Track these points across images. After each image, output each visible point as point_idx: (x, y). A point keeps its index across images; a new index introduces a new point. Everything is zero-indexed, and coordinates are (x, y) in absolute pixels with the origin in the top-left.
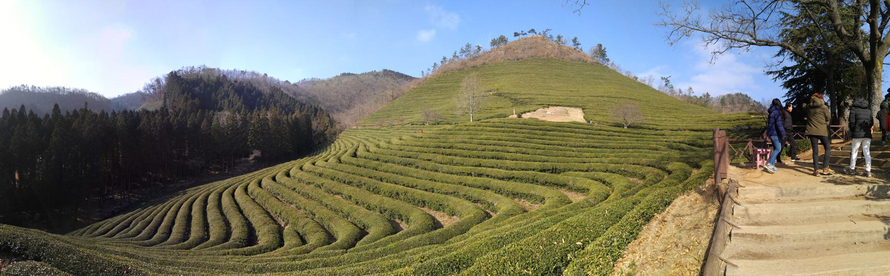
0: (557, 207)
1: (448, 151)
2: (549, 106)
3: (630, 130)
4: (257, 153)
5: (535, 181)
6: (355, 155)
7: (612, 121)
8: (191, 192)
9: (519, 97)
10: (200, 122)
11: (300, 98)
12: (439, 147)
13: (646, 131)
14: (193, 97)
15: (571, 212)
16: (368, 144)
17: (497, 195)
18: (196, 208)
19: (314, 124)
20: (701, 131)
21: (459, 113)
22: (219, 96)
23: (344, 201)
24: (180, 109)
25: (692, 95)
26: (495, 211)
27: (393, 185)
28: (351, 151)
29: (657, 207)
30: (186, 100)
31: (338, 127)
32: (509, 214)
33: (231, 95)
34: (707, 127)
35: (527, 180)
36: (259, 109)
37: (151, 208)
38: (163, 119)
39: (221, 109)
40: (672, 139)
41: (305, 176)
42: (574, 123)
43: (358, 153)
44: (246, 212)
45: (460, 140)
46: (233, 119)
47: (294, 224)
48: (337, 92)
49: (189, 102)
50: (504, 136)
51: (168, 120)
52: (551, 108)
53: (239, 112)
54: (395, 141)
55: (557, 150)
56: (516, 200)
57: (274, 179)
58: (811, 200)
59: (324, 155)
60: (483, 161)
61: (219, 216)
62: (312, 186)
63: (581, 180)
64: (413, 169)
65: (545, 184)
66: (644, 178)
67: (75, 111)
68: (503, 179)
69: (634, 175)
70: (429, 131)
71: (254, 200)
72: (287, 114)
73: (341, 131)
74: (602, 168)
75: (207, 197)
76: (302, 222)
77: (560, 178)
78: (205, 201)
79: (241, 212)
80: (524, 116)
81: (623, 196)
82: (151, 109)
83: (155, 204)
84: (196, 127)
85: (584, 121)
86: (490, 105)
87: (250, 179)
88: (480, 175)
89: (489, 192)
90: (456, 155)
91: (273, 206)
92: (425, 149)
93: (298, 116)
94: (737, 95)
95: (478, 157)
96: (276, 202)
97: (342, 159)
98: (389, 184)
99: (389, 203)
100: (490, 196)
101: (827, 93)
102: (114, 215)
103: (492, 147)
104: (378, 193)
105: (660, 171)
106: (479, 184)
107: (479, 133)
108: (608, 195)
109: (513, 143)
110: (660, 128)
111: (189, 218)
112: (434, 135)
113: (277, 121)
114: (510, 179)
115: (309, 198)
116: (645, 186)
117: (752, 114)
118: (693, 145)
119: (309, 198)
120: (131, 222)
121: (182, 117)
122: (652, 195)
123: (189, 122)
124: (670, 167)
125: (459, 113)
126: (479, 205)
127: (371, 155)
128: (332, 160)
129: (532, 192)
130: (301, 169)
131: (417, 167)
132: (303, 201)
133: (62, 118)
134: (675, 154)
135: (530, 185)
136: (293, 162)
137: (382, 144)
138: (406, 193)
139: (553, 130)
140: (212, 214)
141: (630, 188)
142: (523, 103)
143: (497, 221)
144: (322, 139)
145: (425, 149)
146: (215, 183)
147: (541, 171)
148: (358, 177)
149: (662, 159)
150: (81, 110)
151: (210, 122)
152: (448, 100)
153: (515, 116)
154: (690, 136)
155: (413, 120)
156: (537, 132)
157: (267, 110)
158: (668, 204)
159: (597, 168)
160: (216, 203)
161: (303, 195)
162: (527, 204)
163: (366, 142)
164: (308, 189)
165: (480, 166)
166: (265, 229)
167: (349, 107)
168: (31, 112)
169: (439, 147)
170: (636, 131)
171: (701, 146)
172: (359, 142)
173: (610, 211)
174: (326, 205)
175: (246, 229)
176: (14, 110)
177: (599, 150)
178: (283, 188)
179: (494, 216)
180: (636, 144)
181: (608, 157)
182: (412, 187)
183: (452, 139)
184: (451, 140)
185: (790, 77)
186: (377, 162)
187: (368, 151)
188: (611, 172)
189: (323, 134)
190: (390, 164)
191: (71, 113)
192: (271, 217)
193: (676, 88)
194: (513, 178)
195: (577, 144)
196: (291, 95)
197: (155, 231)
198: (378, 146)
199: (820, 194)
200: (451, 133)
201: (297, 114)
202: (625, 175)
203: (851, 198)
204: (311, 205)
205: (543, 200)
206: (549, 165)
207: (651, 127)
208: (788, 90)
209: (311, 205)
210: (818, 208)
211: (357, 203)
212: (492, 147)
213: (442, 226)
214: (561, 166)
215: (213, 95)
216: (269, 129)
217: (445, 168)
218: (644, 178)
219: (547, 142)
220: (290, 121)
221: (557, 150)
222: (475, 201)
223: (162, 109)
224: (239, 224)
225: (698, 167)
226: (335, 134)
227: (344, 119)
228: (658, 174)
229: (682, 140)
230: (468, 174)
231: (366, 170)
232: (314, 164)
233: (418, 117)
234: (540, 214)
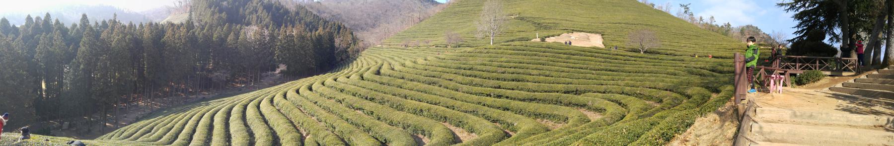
0: (577, 126)
1: (468, 72)
2: (573, 31)
3: (646, 55)
4: (283, 67)
5: (558, 102)
6: (378, 73)
7: (628, 47)
8: (214, 104)
9: (542, 21)
10: (227, 36)
11: (323, 16)
12: (460, 68)
13: (664, 57)
14: (221, 11)
15: (591, 130)
16: (393, 62)
17: (517, 116)
18: (218, 119)
19: (337, 42)
20: (721, 58)
21: (479, 36)
22: (248, 11)
23: (366, 116)
24: (206, 23)
25: (714, 24)
26: (515, 131)
27: (418, 102)
28: (374, 68)
29: (677, 128)
30: (213, 14)
31: (361, 44)
32: (529, 133)
33: (260, 12)
34: (727, 54)
35: (551, 102)
36: (286, 26)
37: (172, 116)
38: (188, 32)
39: (248, 24)
40: (693, 64)
41: (326, 91)
42: (594, 48)
43: (382, 71)
44: (271, 123)
45: (480, 62)
46: (261, 34)
47: (315, 135)
48: (362, 11)
49: (216, 16)
50: (526, 59)
51: (194, 33)
52: (575, 33)
53: (267, 28)
54: (420, 61)
55: (578, 73)
56: (539, 120)
57: (298, 92)
58: (827, 125)
59: (346, 71)
60: (502, 83)
61: (243, 127)
62: (333, 101)
63: (599, 101)
64: (436, 87)
65: (569, 104)
66: (661, 101)
67: (104, 22)
68: (524, 100)
69: (650, 98)
70: (449, 54)
71: (279, 110)
72: (311, 31)
73: (364, 49)
74: (618, 90)
75: (231, 109)
76: (322, 135)
77: (581, 98)
78: (229, 113)
79: (266, 122)
80: (547, 39)
81: (639, 117)
82: (176, 22)
83: (177, 112)
84: (223, 40)
85: (602, 46)
86: (511, 28)
87: (276, 91)
88: (499, 97)
89: (508, 113)
90: (475, 76)
91: (296, 116)
92: (448, 70)
93: (322, 33)
94: (748, 26)
95: (498, 79)
96: (299, 113)
97: (365, 76)
98: (414, 102)
99: (413, 119)
100: (509, 117)
101: (839, 26)
102: (138, 120)
103: (512, 70)
104: (402, 110)
105: (678, 96)
106: (498, 105)
107: (499, 55)
108: (624, 116)
109: (535, 66)
110: (679, 53)
111: (211, 128)
112: (455, 57)
113: (302, 38)
114: (531, 100)
115: (330, 111)
116: (663, 109)
117: (761, 45)
118: (713, 71)
119: (330, 111)
120: (152, 128)
121: (208, 30)
122: (672, 117)
123: (215, 36)
124: (689, 92)
125: (479, 36)
126: (498, 124)
127: (395, 74)
128: (354, 77)
129: (556, 113)
130: (323, 84)
131: (440, 86)
132: (324, 114)
133: (91, 28)
134: (696, 79)
135: (554, 106)
136: (315, 77)
137: (408, 63)
138: (429, 110)
139: (577, 54)
140: (235, 125)
141: (646, 110)
142: (546, 28)
143: (517, 139)
144: (344, 57)
145: (448, 70)
146: (241, 96)
147: (565, 93)
148: (380, 94)
149: (681, 83)
150: (110, 20)
151: (237, 35)
152: (469, 24)
153: (538, 40)
154: (711, 62)
155: (437, 42)
156: (562, 55)
157: (293, 27)
158: (689, 125)
159: (614, 90)
160: (240, 115)
161: (324, 109)
162: (550, 124)
163: (391, 61)
164: (329, 103)
165: (499, 87)
166: (289, 137)
167: (373, 26)
168: (57, 22)
169: (460, 68)
170: (652, 56)
171: (721, 72)
172: (383, 60)
173: (628, 130)
174: (347, 120)
175: (270, 138)
176: (38, 18)
177: (615, 73)
178: (306, 101)
179: (514, 135)
180: (652, 69)
181: (624, 80)
182: (435, 104)
183: (471, 62)
184: (472, 62)
185: (802, 9)
186: (402, 81)
187: (393, 69)
188: (627, 94)
189: (345, 51)
190: (415, 83)
191: (100, 24)
192: (295, 126)
193: (697, 16)
194: (535, 99)
195: (597, 67)
196: (315, 13)
197: (176, 137)
198: (403, 65)
199: (836, 120)
200: (471, 55)
201: (320, 31)
202: (641, 98)
203: (870, 128)
204: (332, 119)
205: (566, 119)
206: (572, 87)
207: (669, 52)
208: (800, 21)
209: (332, 119)
210: (835, 132)
211: (379, 119)
212: (512, 70)
213: (461, 141)
214: (582, 87)
215: (241, 10)
216: (295, 45)
217: (465, 88)
218: (661, 101)
219: (571, 65)
220: (314, 38)
221: (578, 73)
222: (494, 121)
223: (188, 22)
224: (264, 134)
225: (717, 91)
226: (358, 51)
227: (367, 37)
228: (676, 98)
229: (702, 66)
230: (487, 95)
231: (389, 88)
232: (335, 80)
233: (442, 40)
234: (563, 132)
